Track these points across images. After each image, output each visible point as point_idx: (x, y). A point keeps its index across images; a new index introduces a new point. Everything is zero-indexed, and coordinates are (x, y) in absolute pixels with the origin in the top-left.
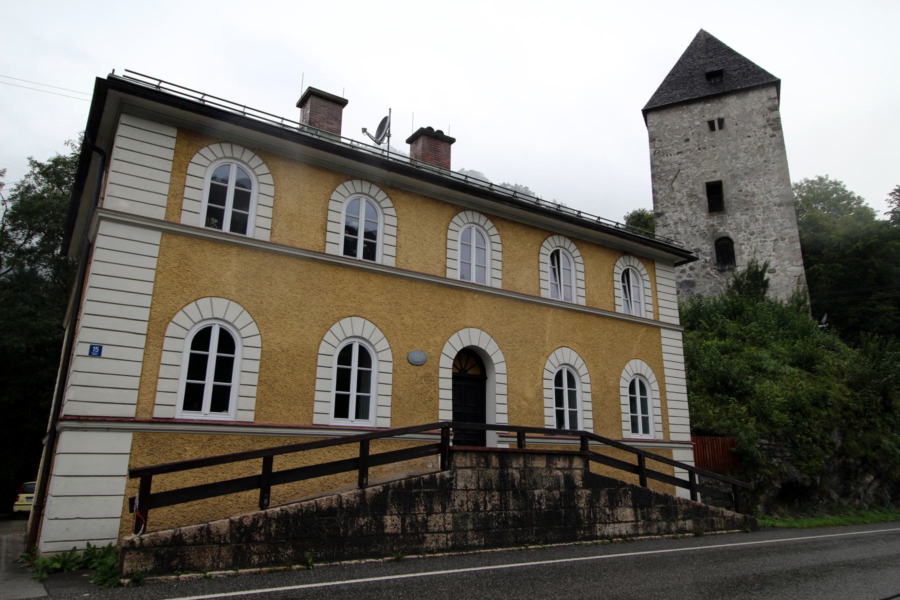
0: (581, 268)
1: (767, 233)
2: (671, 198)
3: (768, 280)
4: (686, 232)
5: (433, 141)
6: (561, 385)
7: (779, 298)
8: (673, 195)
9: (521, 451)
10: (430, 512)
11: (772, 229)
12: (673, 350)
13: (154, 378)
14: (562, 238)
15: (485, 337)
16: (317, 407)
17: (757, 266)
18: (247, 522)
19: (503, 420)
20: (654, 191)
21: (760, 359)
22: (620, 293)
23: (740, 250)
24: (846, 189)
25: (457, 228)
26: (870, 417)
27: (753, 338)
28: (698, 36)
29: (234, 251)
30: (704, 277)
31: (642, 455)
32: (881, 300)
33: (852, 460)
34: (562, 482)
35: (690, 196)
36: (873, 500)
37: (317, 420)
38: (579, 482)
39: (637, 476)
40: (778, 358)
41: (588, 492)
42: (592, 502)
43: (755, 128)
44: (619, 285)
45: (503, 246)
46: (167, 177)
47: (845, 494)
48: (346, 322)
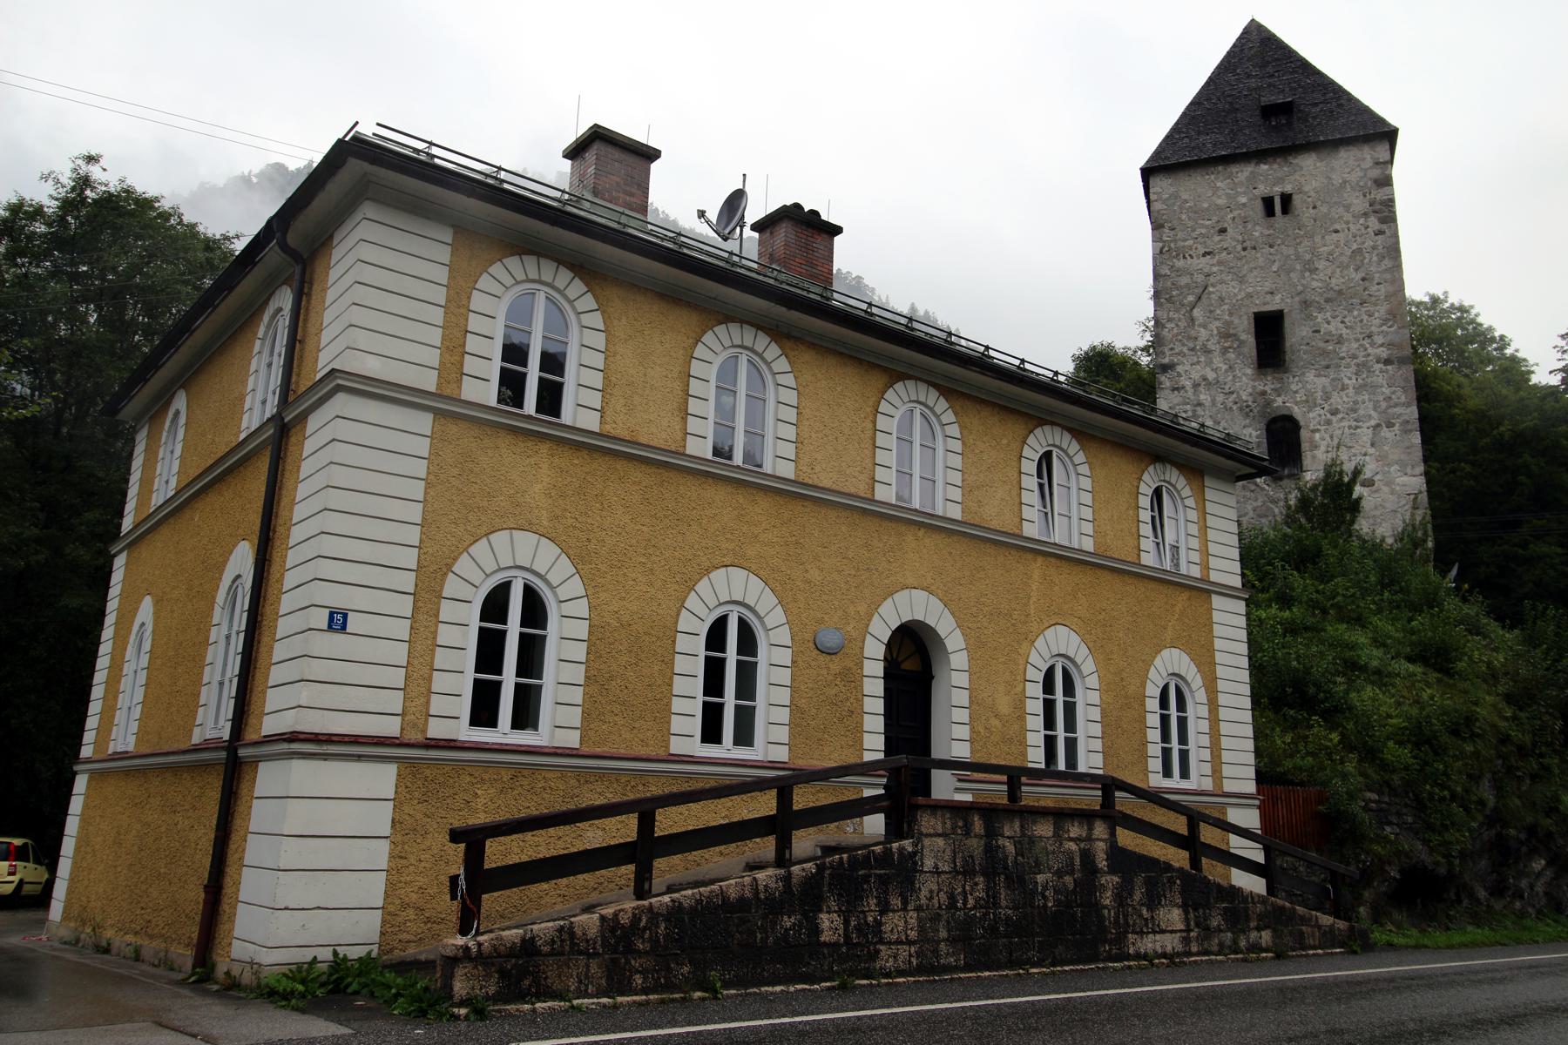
0: (1086, 483)
1: (1361, 412)
2: (1189, 338)
3: (1360, 498)
4: (1214, 402)
5: (805, 230)
6: (722, 648)
8: (1193, 333)
9: (1014, 809)
10: (885, 908)
11: (1371, 405)
12: (1230, 632)
13: (426, 670)
14: (1057, 430)
15: (936, 604)
16: (677, 724)
17: (1341, 473)
18: (625, 920)
19: (961, 751)
21: (1353, 647)
22: (1032, 498)
23: (1312, 441)
24: (1479, 320)
25: (708, 356)
26: (1541, 755)
27: (1338, 607)
28: (1246, 31)
29: (544, 448)
31: (1195, 818)
33: (1512, 832)
34: (1077, 861)
35: (1225, 335)
37: (677, 746)
38: (1102, 864)
39: (1185, 854)
40: (1384, 645)
41: (1116, 879)
42: (1121, 897)
44: (1031, 482)
45: (964, 443)
46: (437, 315)
47: (1498, 890)
48: (718, 575)
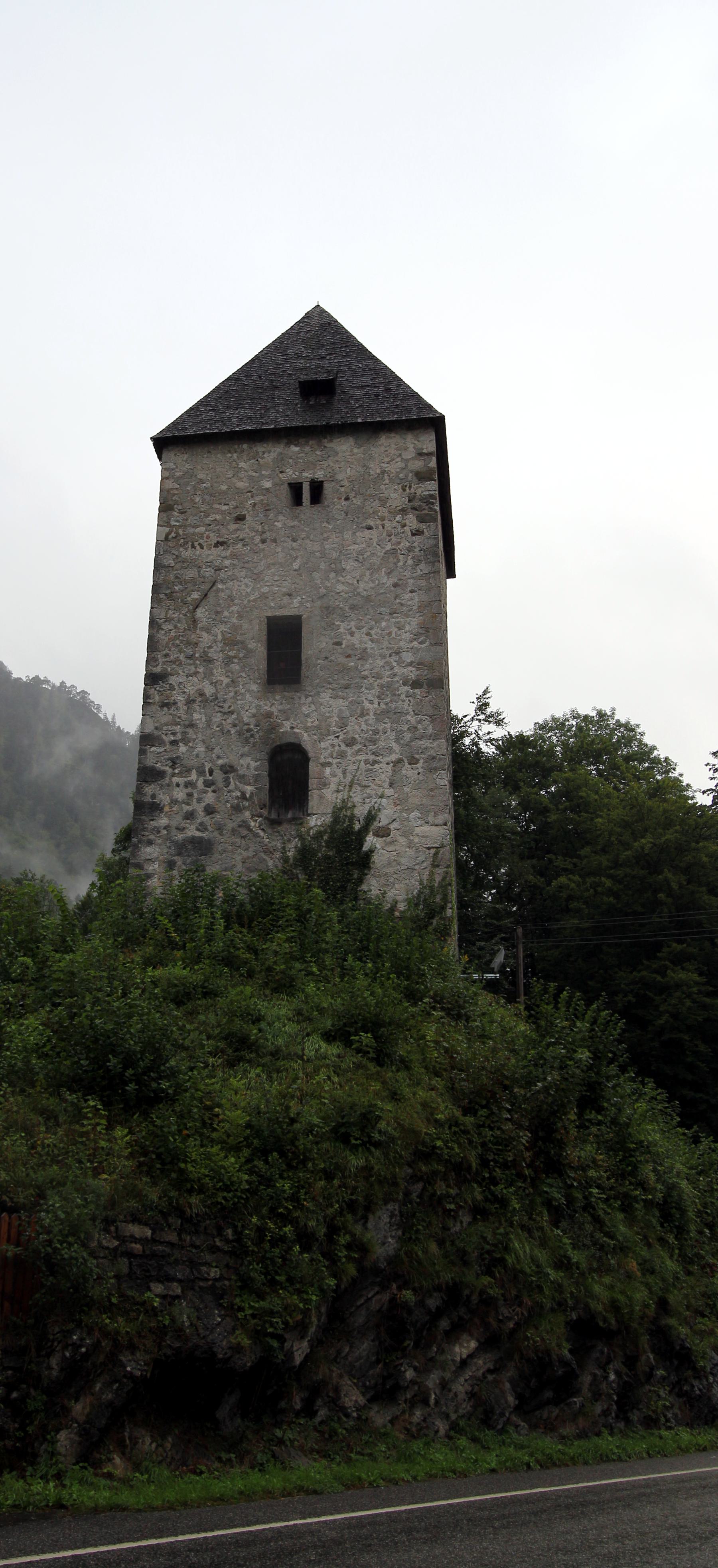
1: (381, 744)
2: (188, 643)
3: (371, 851)
4: (209, 723)
7: (391, 894)
8: (193, 637)
11: (393, 736)
17: (352, 818)
20: (153, 624)
23: (321, 777)
28: (308, 316)
30: (233, 831)
32: (679, 960)
36: (466, 1407)
43: (383, 512)
47: (385, 1391)
